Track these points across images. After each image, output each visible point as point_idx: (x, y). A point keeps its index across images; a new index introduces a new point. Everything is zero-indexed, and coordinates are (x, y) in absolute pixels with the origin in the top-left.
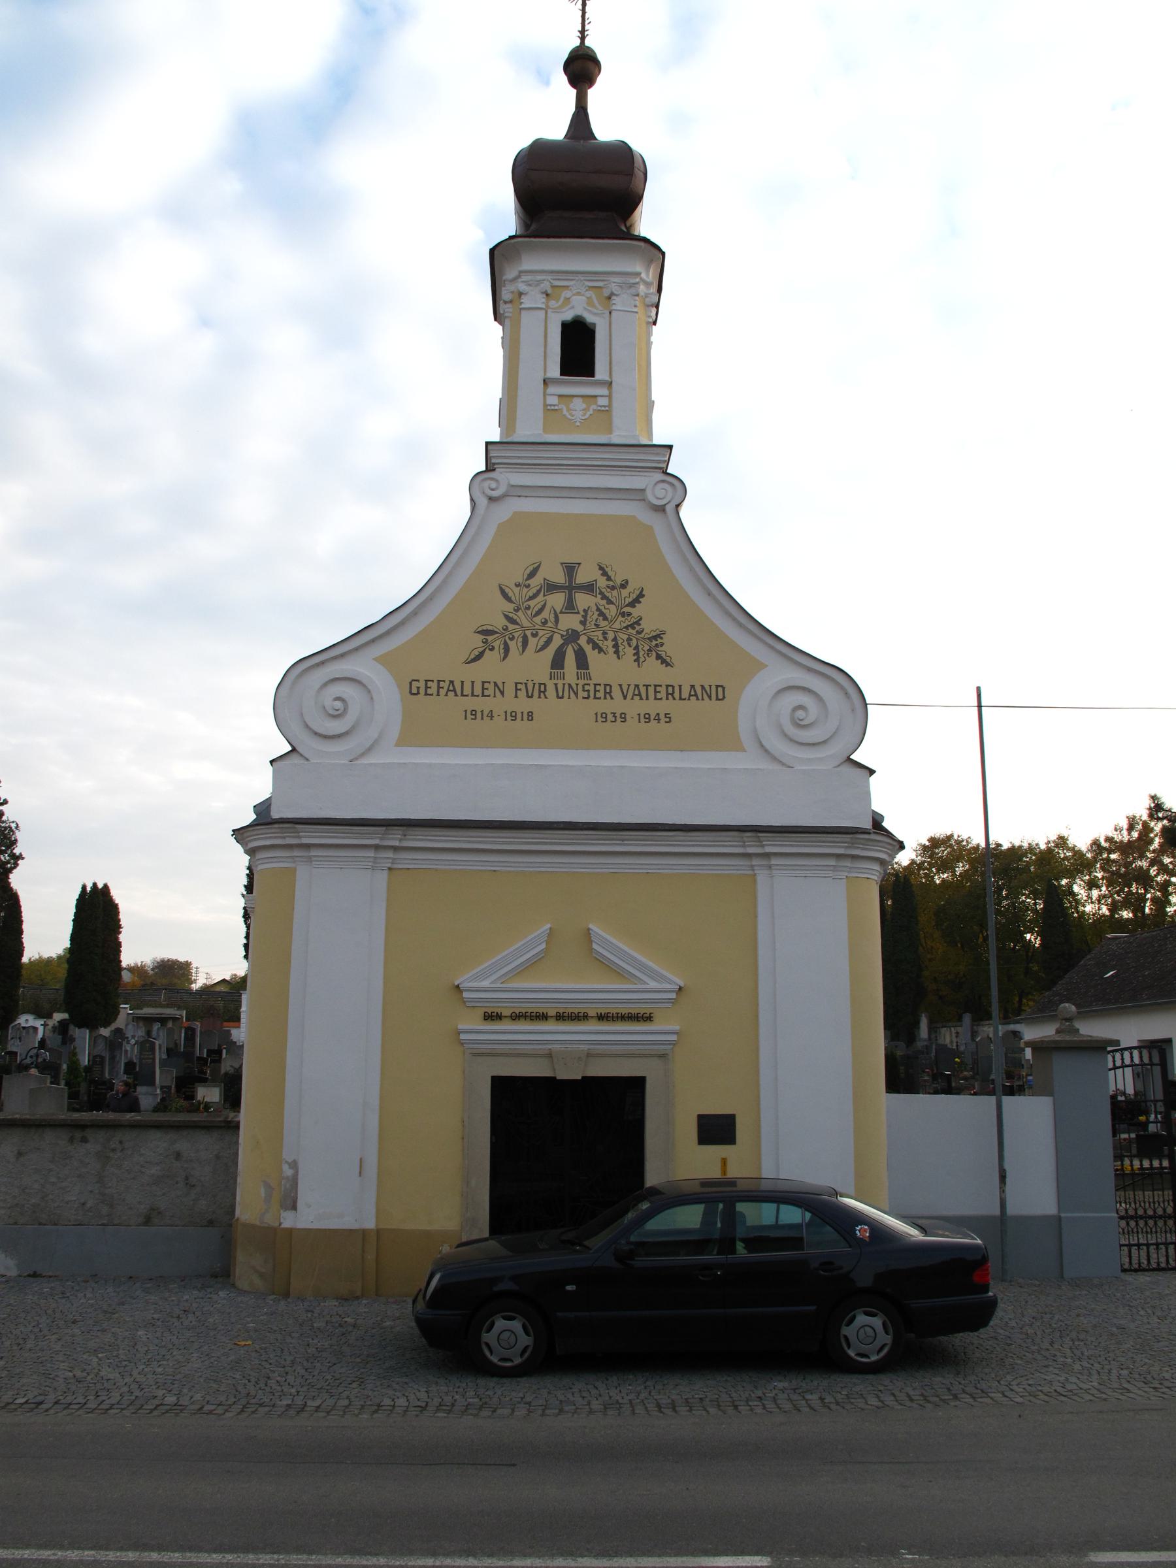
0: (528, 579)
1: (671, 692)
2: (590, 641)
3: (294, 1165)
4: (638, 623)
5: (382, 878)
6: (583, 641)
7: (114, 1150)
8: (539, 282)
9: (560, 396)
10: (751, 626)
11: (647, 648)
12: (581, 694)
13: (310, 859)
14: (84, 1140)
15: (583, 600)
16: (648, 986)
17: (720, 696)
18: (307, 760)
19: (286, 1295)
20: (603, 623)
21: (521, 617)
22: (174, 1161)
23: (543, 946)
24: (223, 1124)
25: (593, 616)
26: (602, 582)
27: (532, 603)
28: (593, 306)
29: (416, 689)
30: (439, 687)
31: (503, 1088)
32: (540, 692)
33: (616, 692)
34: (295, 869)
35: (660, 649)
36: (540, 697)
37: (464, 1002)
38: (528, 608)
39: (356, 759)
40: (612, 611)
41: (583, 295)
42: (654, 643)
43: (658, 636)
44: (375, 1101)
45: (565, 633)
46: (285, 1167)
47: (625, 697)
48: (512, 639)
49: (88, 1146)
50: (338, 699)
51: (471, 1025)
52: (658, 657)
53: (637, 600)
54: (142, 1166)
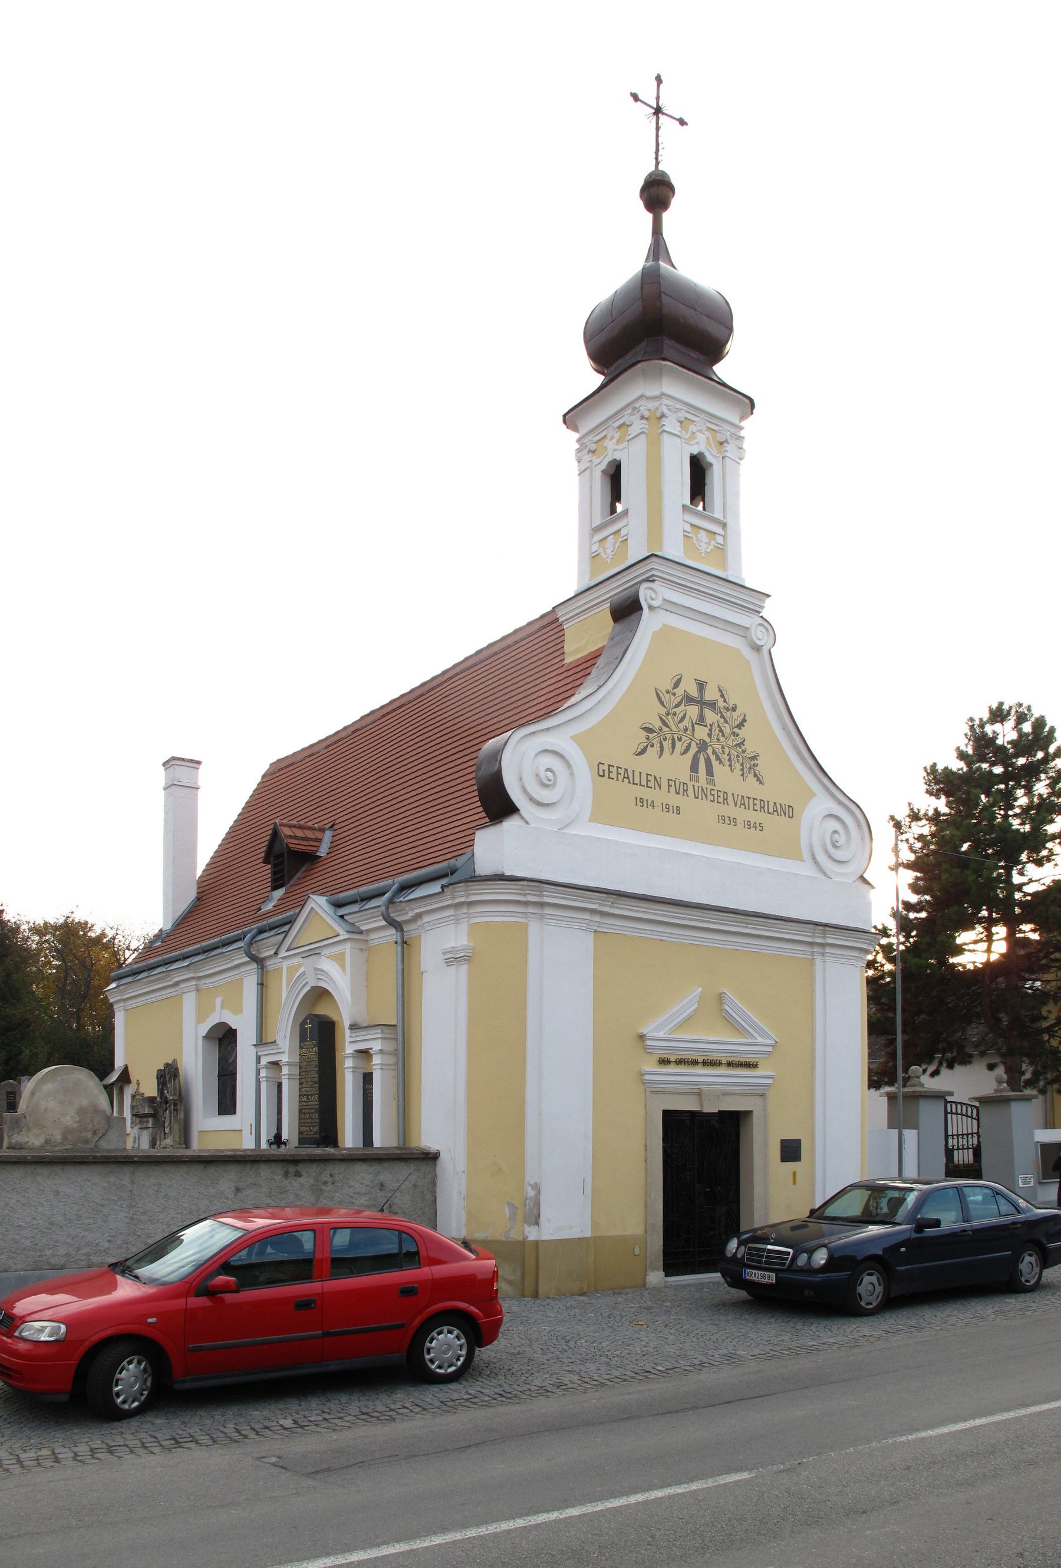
0: (674, 688)
1: (763, 806)
2: (714, 752)
3: (536, 1187)
4: (742, 743)
5: (587, 941)
6: (710, 751)
7: (325, 1183)
8: (679, 410)
9: (692, 525)
10: (810, 761)
11: (748, 766)
12: (710, 797)
13: (542, 917)
14: (298, 1174)
15: (710, 716)
16: (757, 1041)
17: (791, 816)
18: (527, 823)
19: (536, 1295)
20: (722, 739)
21: (670, 720)
22: (378, 1191)
23: (696, 1005)
24: (423, 1156)
25: (716, 731)
26: (721, 703)
27: (677, 710)
28: (710, 446)
29: (604, 772)
30: (618, 774)
31: (671, 1119)
32: (684, 790)
33: (730, 800)
34: (526, 925)
35: (756, 768)
36: (683, 795)
37: (645, 1048)
38: (675, 714)
39: (562, 828)
40: (727, 729)
41: (704, 434)
42: (753, 762)
43: (754, 758)
44: (590, 1133)
45: (698, 742)
46: (529, 1189)
47: (736, 806)
48: (665, 739)
49: (302, 1180)
50: (548, 770)
51: (650, 1066)
52: (755, 775)
53: (740, 725)
54: (351, 1197)
